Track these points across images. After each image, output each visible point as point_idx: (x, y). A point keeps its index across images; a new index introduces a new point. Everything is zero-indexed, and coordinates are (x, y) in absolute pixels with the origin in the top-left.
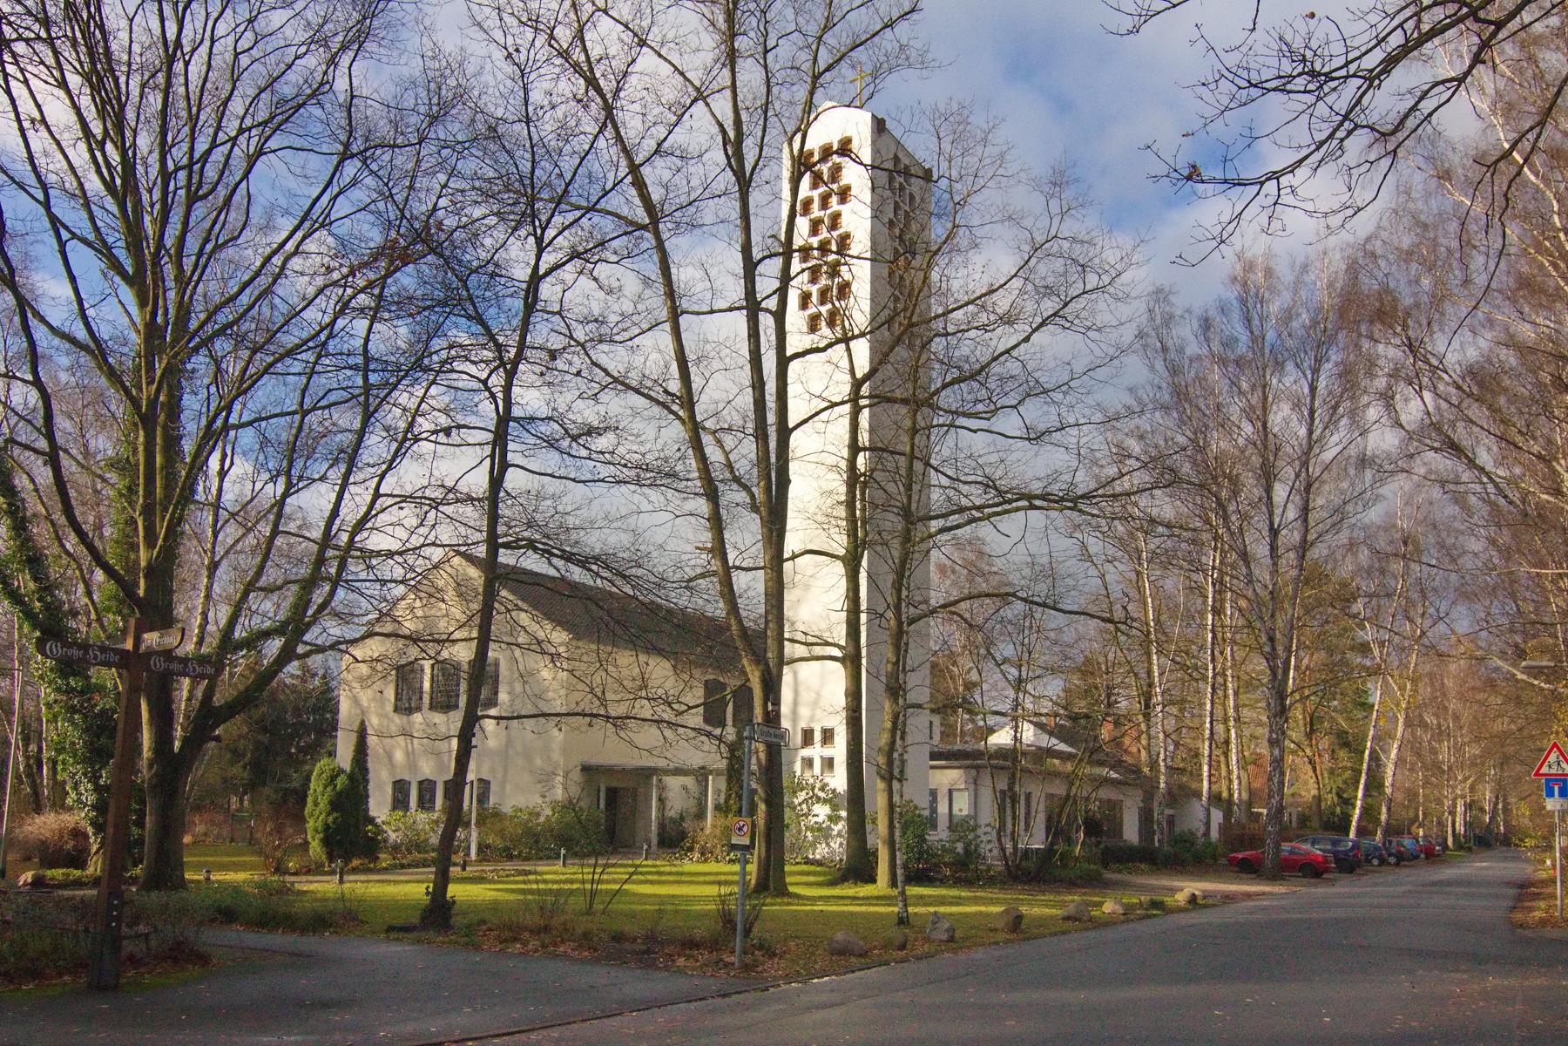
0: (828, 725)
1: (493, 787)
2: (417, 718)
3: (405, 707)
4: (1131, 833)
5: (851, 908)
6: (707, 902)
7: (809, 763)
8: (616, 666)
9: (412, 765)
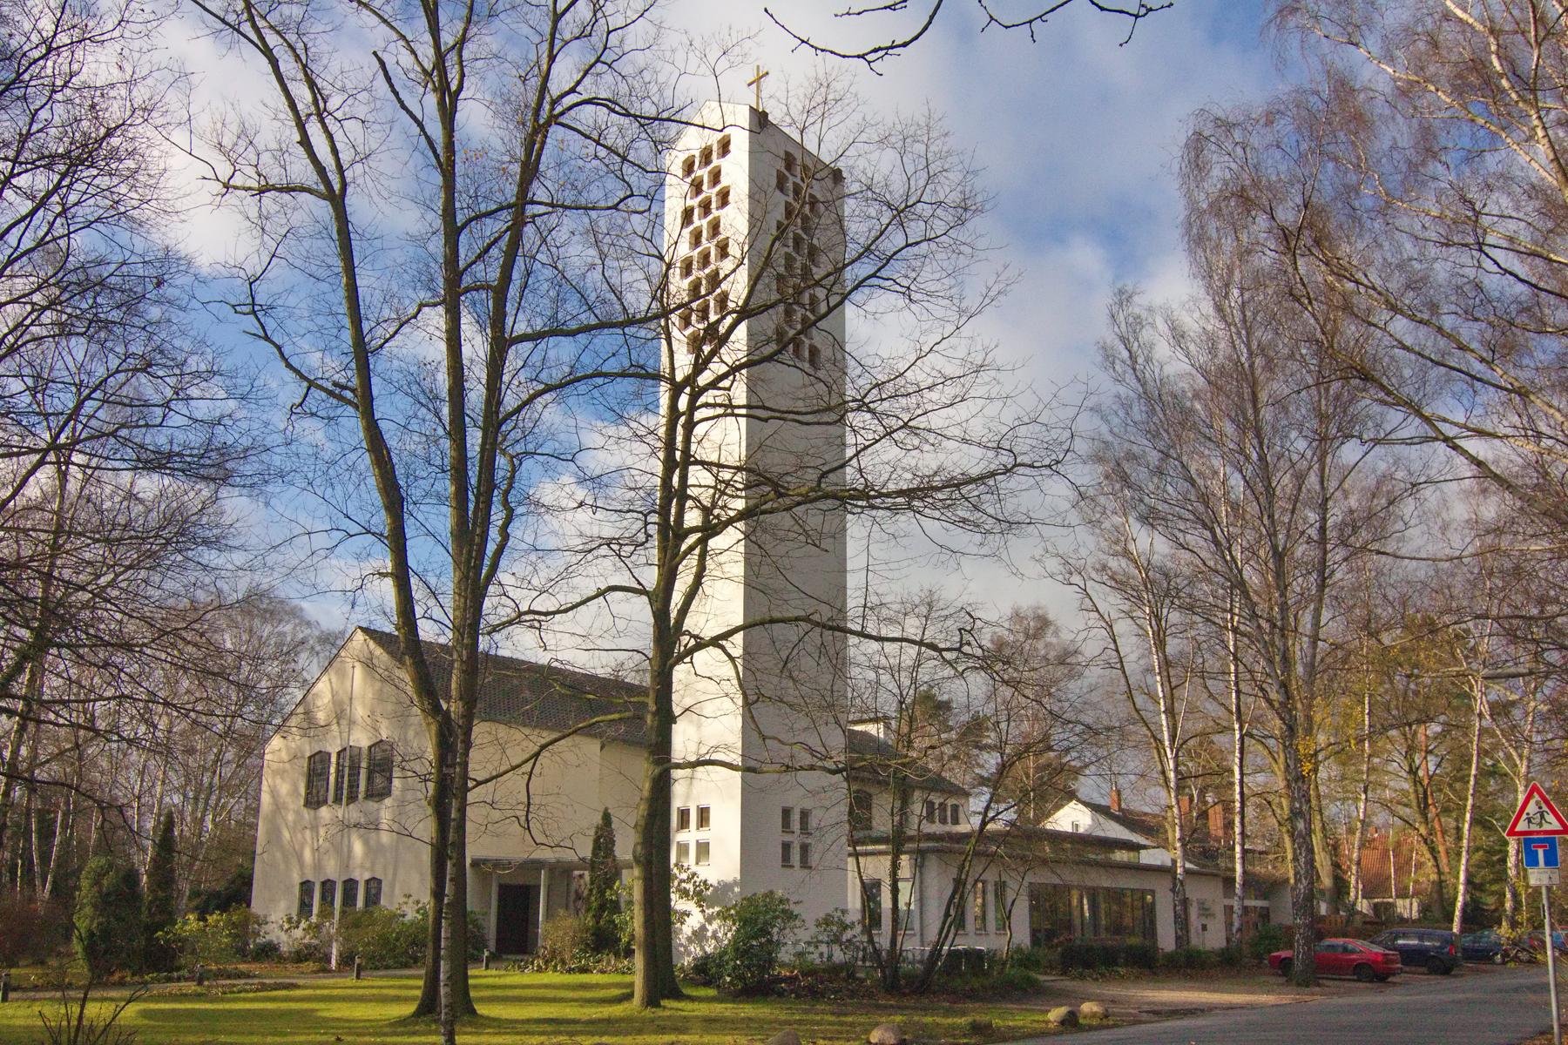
0: (704, 804)
1: (385, 888)
2: (324, 812)
3: (314, 801)
4: (1166, 940)
5: (197, 1006)
6: (466, 1033)
7: (683, 849)
8: (982, 767)
9: (318, 866)
